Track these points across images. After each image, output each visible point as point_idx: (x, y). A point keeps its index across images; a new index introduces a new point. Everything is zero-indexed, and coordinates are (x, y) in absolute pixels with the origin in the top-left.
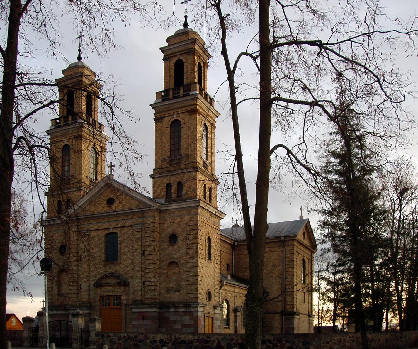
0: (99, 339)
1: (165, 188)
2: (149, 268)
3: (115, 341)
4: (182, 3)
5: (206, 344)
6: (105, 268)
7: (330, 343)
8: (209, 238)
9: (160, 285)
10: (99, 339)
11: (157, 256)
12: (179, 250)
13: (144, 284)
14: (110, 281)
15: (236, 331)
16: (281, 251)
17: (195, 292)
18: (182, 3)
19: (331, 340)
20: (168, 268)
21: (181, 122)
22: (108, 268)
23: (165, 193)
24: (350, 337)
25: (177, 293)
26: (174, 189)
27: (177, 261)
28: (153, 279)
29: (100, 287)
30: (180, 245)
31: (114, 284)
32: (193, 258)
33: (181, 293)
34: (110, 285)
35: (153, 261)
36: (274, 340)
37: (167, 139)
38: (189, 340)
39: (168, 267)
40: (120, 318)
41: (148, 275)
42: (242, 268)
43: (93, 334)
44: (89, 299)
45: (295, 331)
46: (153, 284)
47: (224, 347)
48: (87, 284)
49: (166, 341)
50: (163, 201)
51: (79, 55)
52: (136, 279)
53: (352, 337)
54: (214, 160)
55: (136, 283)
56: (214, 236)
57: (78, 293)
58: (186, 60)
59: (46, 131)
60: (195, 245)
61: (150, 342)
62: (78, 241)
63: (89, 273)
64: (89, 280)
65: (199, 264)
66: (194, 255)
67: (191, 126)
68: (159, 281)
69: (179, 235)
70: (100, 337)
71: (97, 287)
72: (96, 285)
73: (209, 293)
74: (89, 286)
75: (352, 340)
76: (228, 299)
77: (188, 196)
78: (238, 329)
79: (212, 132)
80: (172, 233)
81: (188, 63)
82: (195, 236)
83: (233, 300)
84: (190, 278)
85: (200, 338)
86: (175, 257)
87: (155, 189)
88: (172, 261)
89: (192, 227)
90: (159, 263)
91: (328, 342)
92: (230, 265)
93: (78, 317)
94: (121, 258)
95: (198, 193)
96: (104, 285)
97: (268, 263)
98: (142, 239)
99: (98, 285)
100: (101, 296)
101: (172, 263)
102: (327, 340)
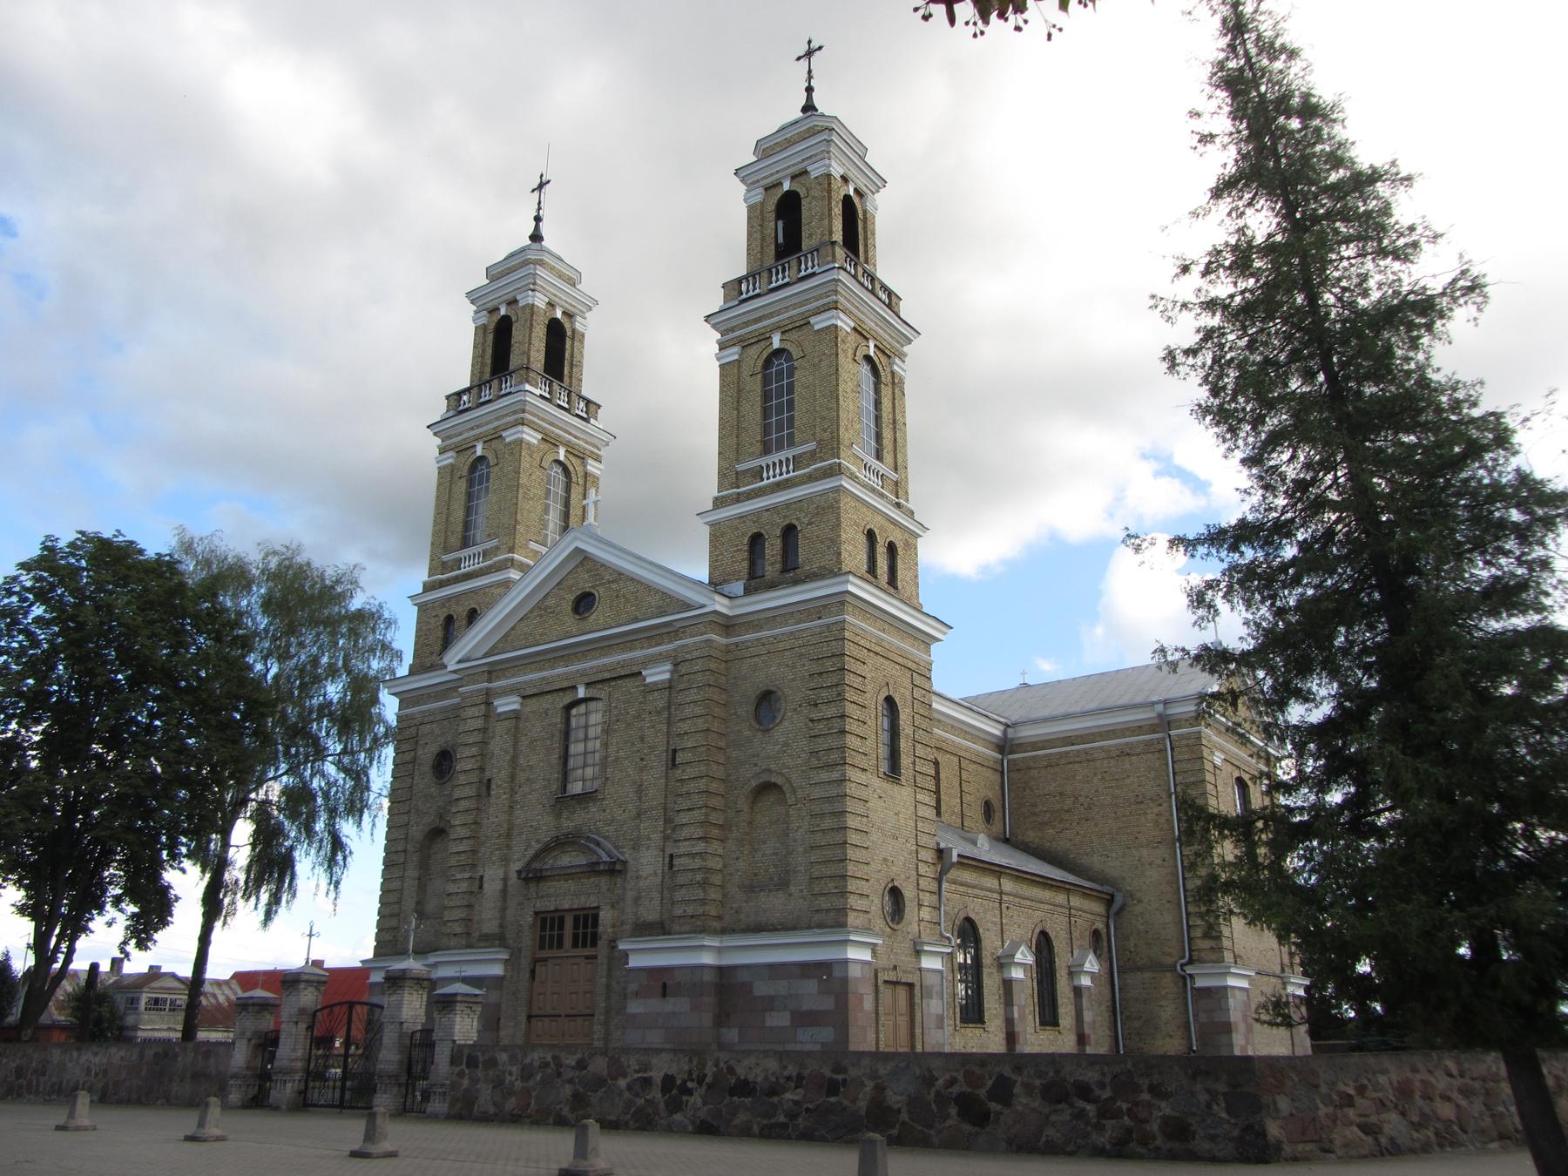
0: (461, 1075)
1: (746, 548)
2: (689, 810)
3: (512, 1083)
4: (799, 59)
5: (833, 1099)
6: (558, 816)
7: (1359, 1101)
8: (890, 701)
9: (724, 866)
10: (461, 1075)
11: (715, 767)
12: (786, 744)
13: (671, 866)
14: (569, 859)
15: (1011, 1038)
16: (1160, 751)
17: (836, 888)
18: (799, 59)
19: (1361, 1090)
20: (752, 808)
21: (793, 353)
22: (564, 816)
23: (745, 564)
24: (1450, 1075)
25: (780, 894)
26: (773, 548)
27: (779, 781)
28: (700, 847)
29: (538, 882)
30: (791, 723)
31: (578, 870)
32: (830, 766)
33: (790, 895)
34: (567, 874)
35: (702, 784)
36: (1102, 1085)
37: (752, 406)
38: (766, 1078)
39: (753, 803)
40: (591, 992)
41: (685, 833)
42: (1036, 814)
43: (442, 1055)
44: (501, 926)
45: (1234, 1035)
46: (698, 863)
47: (899, 1111)
48: (501, 873)
49: (684, 1082)
50: (737, 587)
51: (537, 228)
52: (648, 849)
53: (1462, 1076)
54: (905, 461)
55: (647, 864)
56: (908, 693)
57: (470, 906)
58: (808, 190)
59: (428, 427)
60: (836, 724)
61: (629, 1088)
62: (484, 733)
63: (509, 835)
64: (505, 860)
65: (851, 789)
66: (834, 756)
67: (821, 360)
68: (720, 851)
69: (787, 691)
70: (464, 1066)
71: (526, 880)
72: (523, 876)
73: (895, 893)
74: (505, 880)
75: (1461, 1091)
76: (972, 916)
77: (815, 567)
78: (1016, 1029)
79: (893, 383)
80: (765, 688)
81: (813, 197)
82: (834, 692)
83: (997, 920)
84: (821, 840)
85: (806, 1072)
86: (773, 766)
87: (717, 556)
88: (761, 780)
89: (828, 665)
90: (721, 790)
91: (1350, 1096)
92: (996, 804)
93: (401, 987)
94: (607, 779)
95: (844, 555)
96: (549, 874)
97: (1118, 792)
98: (670, 714)
99: (533, 876)
100: (536, 913)
101: (766, 788)
102: (1341, 1087)
